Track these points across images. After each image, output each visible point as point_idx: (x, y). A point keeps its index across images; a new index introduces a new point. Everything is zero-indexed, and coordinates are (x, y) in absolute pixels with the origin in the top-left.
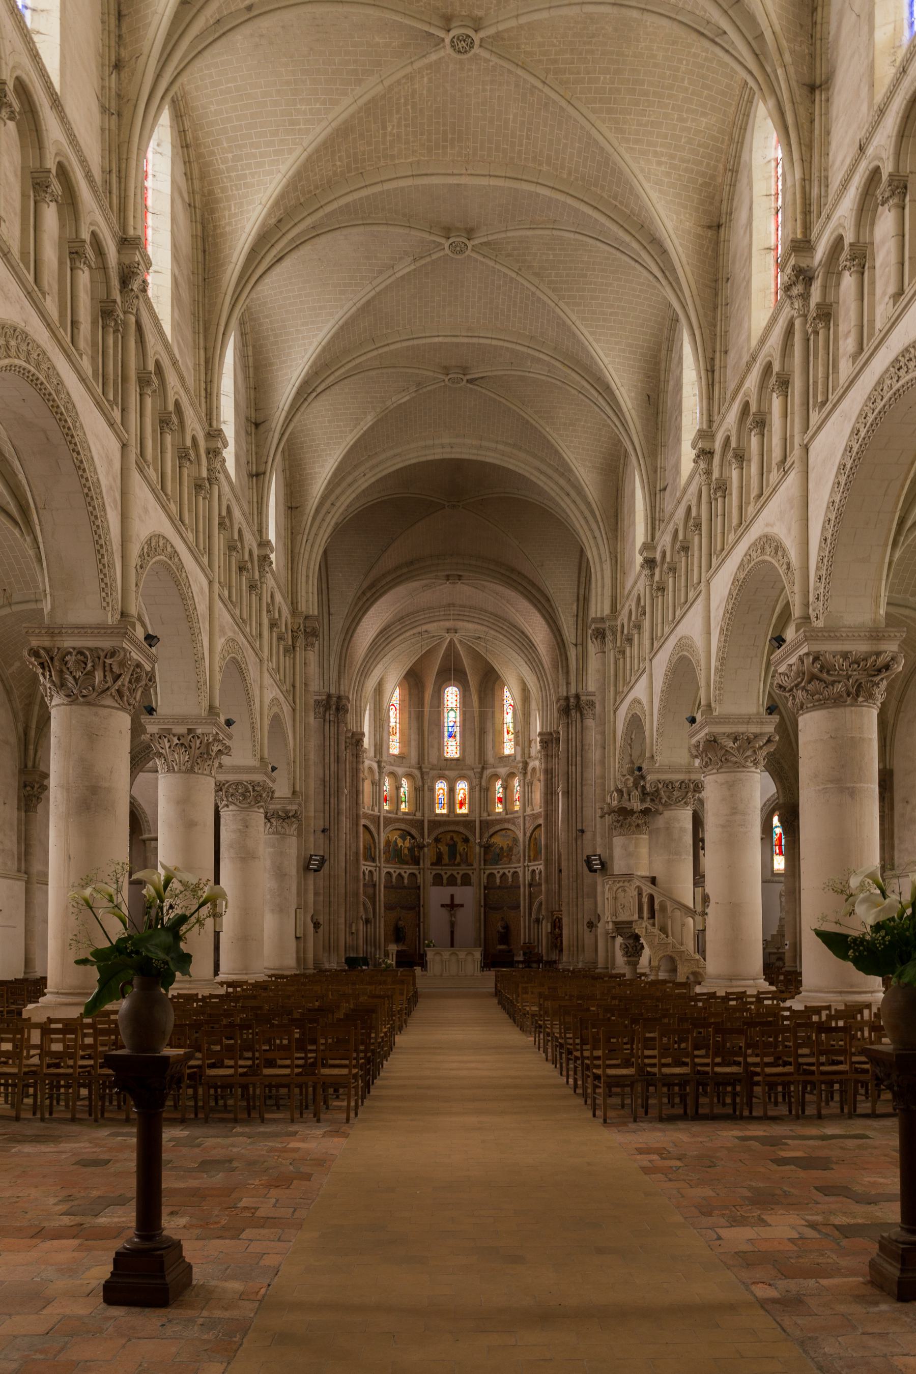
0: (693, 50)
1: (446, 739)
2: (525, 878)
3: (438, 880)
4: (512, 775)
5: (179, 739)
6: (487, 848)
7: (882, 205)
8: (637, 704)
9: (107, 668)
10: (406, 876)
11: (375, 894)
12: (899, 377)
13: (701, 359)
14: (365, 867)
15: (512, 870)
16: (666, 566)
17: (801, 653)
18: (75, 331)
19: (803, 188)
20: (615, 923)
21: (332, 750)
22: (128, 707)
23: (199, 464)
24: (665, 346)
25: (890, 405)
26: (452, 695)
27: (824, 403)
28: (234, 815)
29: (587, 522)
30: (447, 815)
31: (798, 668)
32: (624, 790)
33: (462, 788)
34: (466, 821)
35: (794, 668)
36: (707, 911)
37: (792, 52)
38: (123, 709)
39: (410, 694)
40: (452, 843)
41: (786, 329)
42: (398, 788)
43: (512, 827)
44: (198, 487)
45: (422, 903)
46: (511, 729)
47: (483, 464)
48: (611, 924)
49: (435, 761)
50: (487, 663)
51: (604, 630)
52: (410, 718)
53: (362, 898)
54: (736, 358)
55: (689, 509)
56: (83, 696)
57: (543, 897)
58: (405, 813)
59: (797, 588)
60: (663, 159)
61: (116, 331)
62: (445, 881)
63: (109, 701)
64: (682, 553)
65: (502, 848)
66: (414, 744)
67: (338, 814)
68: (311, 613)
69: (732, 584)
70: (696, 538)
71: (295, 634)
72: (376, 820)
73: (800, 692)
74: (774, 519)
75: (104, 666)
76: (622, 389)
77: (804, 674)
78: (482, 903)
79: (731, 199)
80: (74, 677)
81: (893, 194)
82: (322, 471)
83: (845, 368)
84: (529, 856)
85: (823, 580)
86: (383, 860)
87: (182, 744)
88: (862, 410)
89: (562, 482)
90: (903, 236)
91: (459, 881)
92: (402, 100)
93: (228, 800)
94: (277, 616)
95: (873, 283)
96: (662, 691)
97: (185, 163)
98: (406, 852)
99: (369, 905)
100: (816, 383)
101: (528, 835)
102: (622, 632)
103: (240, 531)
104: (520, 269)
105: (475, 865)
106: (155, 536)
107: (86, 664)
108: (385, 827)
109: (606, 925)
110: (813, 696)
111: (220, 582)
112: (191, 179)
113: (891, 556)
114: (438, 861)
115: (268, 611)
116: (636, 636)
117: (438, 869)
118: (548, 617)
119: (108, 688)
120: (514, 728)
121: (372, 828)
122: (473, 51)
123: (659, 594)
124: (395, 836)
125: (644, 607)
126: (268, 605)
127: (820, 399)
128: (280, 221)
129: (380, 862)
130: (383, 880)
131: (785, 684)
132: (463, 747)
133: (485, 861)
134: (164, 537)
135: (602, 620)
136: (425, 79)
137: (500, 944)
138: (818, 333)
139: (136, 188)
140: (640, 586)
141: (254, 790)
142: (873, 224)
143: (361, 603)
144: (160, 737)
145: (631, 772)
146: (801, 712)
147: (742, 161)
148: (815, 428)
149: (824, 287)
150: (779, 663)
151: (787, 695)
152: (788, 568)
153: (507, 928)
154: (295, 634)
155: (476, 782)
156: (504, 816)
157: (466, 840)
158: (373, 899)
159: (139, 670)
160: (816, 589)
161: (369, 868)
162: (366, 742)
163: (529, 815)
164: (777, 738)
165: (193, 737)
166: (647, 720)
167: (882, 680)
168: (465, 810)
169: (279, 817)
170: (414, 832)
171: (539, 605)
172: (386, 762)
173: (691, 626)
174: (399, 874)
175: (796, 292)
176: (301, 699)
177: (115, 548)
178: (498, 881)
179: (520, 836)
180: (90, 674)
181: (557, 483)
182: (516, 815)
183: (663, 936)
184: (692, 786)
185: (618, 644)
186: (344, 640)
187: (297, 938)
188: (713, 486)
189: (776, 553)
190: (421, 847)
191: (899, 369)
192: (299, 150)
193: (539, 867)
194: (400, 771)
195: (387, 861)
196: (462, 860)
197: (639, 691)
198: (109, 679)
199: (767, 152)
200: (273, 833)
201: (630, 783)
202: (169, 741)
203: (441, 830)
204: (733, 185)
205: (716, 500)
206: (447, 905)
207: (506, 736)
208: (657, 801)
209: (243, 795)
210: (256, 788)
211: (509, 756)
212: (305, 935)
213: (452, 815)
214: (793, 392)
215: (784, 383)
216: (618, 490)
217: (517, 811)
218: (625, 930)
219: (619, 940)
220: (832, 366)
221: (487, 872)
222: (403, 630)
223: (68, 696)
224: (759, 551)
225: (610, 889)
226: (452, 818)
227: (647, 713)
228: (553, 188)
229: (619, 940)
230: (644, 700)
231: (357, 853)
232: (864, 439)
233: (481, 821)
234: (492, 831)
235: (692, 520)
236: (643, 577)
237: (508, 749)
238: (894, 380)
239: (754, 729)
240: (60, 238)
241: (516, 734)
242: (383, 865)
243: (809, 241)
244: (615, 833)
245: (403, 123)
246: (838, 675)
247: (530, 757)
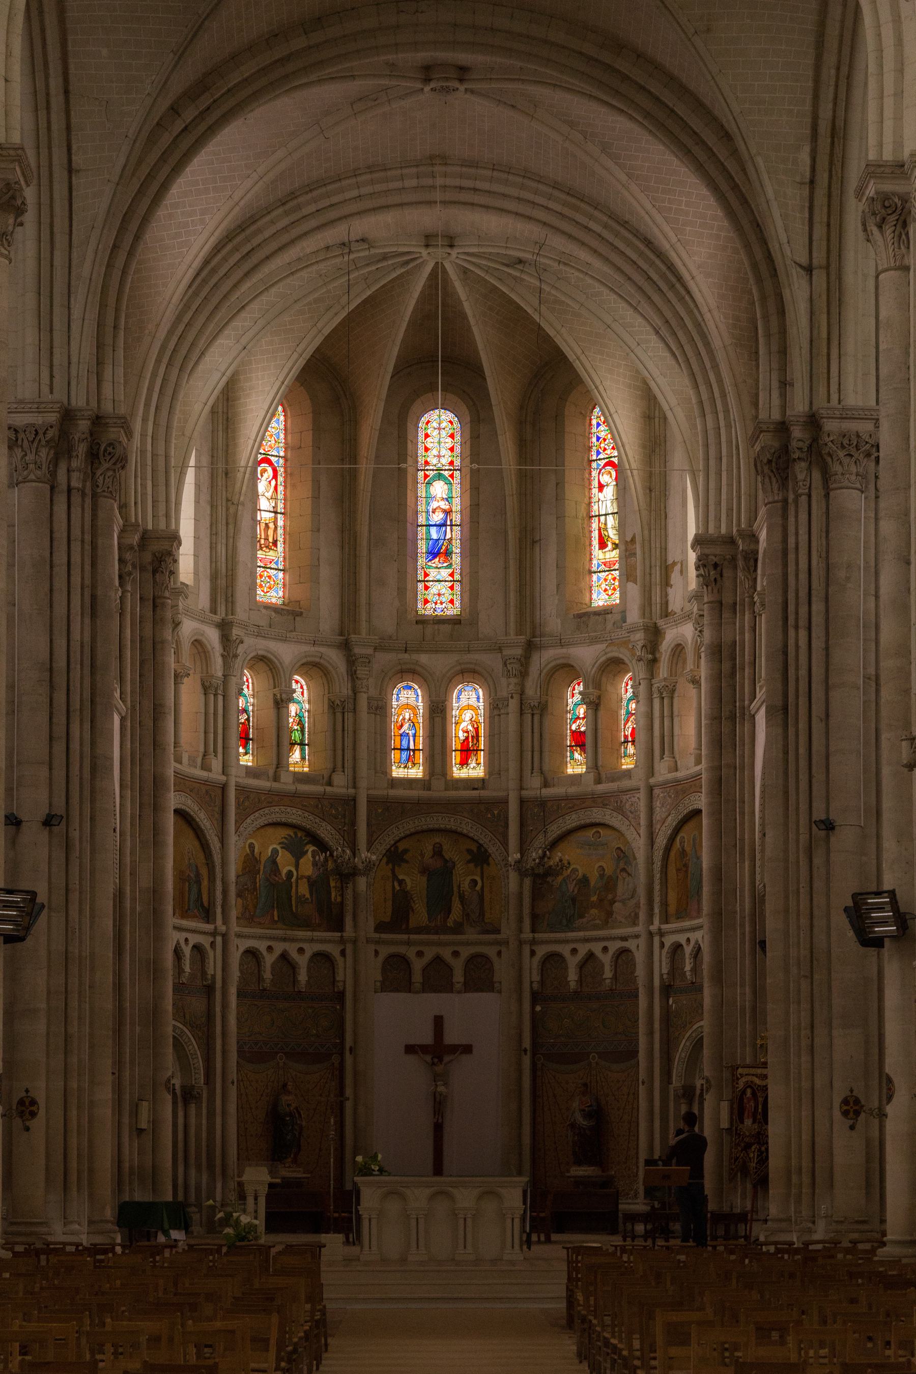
1: (421, 561)
3: (396, 976)
10: (302, 961)
15: (614, 946)
26: (439, 435)
33: (468, 706)
34: (480, 802)
43: (615, 820)
45: (349, 1042)
46: (613, 534)
52: (316, 498)
62: (417, 977)
65: (585, 881)
66: (328, 573)
78: (527, 1043)
84: (665, 904)
86: (234, 914)
91: (458, 977)
98: (304, 889)
99: (193, 1047)
101: (661, 841)
105: (507, 931)
114: (398, 919)
121: (203, 819)
124: (271, 845)
129: (225, 921)
132: (471, 583)
133: (534, 917)
137: (579, 1163)
153: (597, 1114)
155: (508, 686)
156: (590, 786)
157: (480, 857)
161: (194, 939)
163: (664, 785)
168: (475, 770)
170: (326, 831)
174: (284, 956)
176: (225, 1006)
178: (572, 976)
179: (639, 845)
194: (286, 653)
195: (248, 918)
206: (424, 1049)
207: (599, 556)
221: (542, 951)
226: (439, 792)
233: (522, 802)
237: (603, 593)
241: (627, 547)
242: (235, 928)
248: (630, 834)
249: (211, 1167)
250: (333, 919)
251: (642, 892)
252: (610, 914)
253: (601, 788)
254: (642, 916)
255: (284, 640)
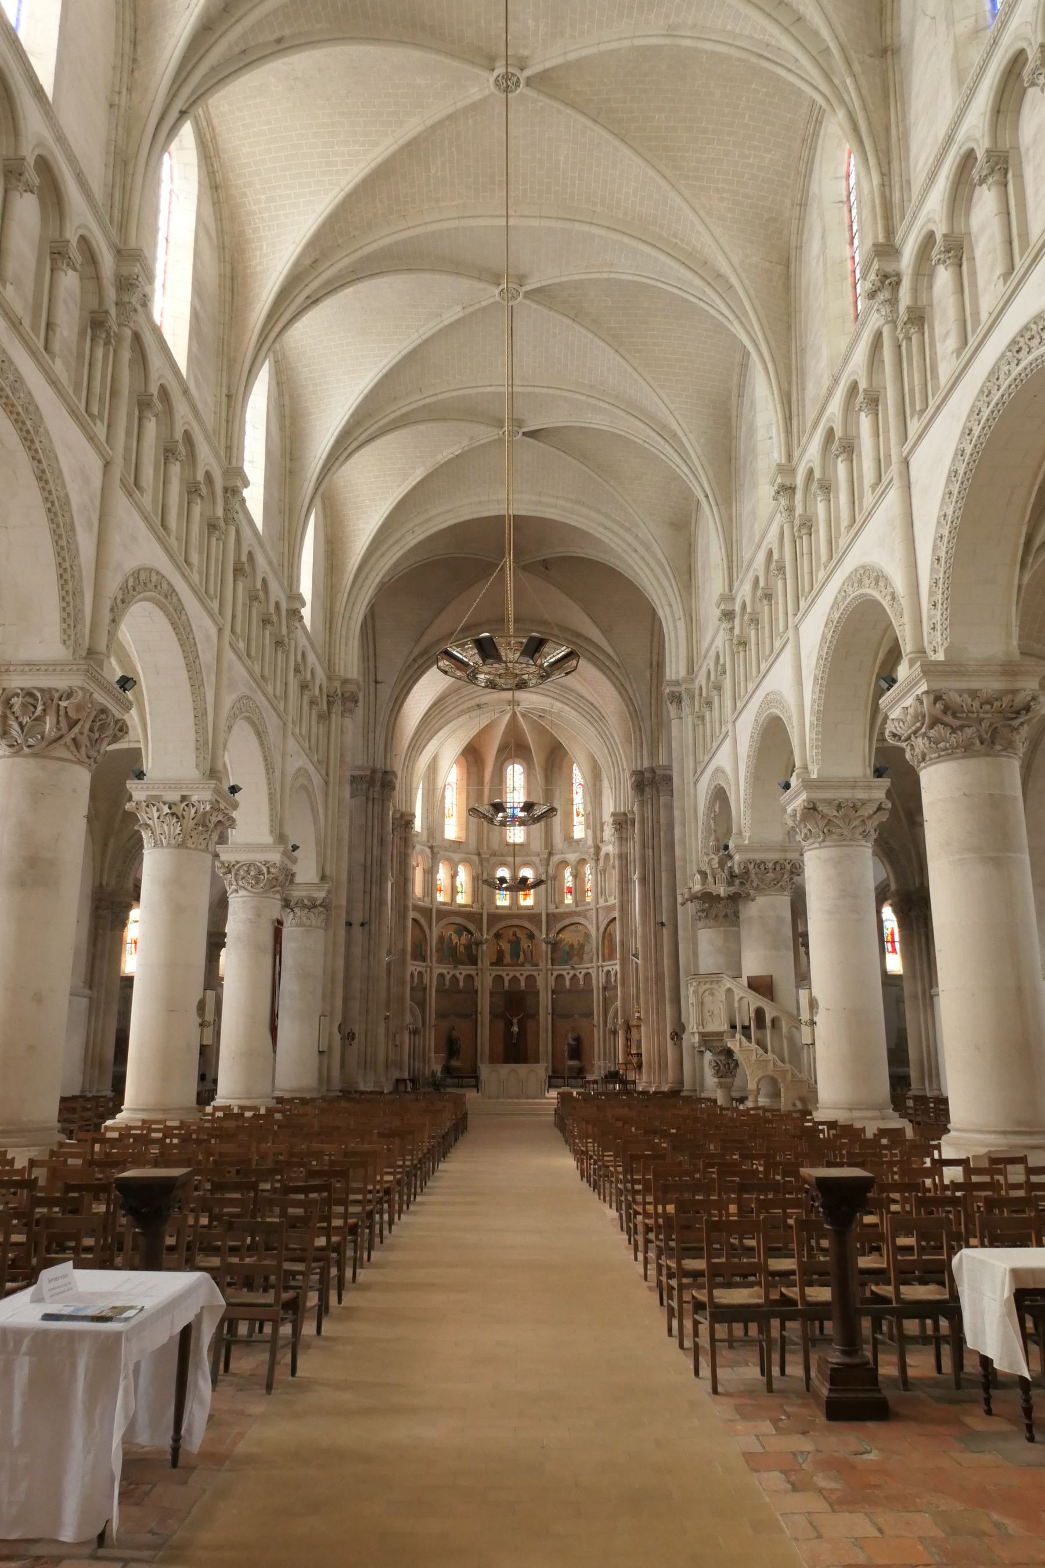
0: (753, 86)
2: (598, 980)
4: (582, 861)
5: (170, 808)
6: (555, 945)
7: (980, 185)
8: (720, 774)
9: (62, 713)
10: (461, 978)
11: (424, 999)
12: (1019, 361)
13: (776, 392)
14: (414, 968)
15: (584, 971)
16: (746, 617)
17: (919, 692)
18: (50, 332)
19: (883, 195)
20: (703, 1035)
21: (376, 832)
22: (87, 760)
23: (214, 502)
24: (735, 392)
25: (1010, 394)
27: (923, 411)
28: (244, 902)
29: (658, 579)
30: (510, 908)
31: (916, 710)
32: (708, 871)
35: (911, 711)
36: (815, 1019)
37: (862, 63)
38: (80, 763)
39: (468, 772)
40: (514, 939)
41: (872, 344)
42: (453, 877)
44: (212, 527)
46: (582, 811)
47: (543, 521)
48: (697, 1036)
49: (495, 845)
50: (552, 735)
51: (680, 694)
53: (408, 1003)
54: (814, 388)
55: (770, 553)
56: (29, 746)
57: (619, 1003)
58: (461, 906)
59: (906, 618)
60: (725, 195)
61: (107, 343)
63: (65, 754)
64: (765, 602)
67: (380, 904)
68: (350, 676)
69: (826, 626)
70: (780, 583)
71: (331, 699)
72: (427, 912)
73: (920, 739)
74: (875, 547)
75: (58, 710)
76: (691, 436)
77: (924, 717)
78: (550, 1011)
79: (800, 232)
80: (20, 724)
81: (992, 171)
82: (364, 527)
83: (946, 370)
84: (603, 955)
85: (939, 606)
87: (173, 814)
88: (973, 406)
89: (630, 538)
90: (1008, 214)
92: (446, 143)
93: (237, 884)
94: (309, 676)
95: (973, 274)
96: (749, 756)
97: (214, 204)
98: (462, 949)
99: (418, 1012)
100: (912, 391)
101: (602, 930)
102: (701, 695)
103: (303, 654)
104: (576, 316)
105: (542, 965)
106: (146, 569)
107: (35, 707)
108: (438, 920)
109: (691, 1038)
110: (937, 743)
111: (233, 631)
112: (221, 220)
113: (1020, 579)
114: (499, 961)
115: (297, 670)
116: (716, 698)
117: (498, 971)
118: (618, 685)
119: (61, 737)
120: (585, 809)
121: (423, 921)
122: (519, 90)
123: (741, 648)
124: (450, 932)
125: (724, 666)
126: (296, 664)
127: (919, 403)
128: (316, 261)
130: (435, 982)
131: (899, 732)
133: (552, 959)
134: (158, 573)
135: (677, 683)
136: (470, 121)
138: (910, 339)
139: (396, 542)
140: (719, 642)
141: (269, 872)
142: (968, 214)
143: (411, 671)
144: (147, 806)
145: (717, 850)
146: (923, 765)
147: (811, 193)
148: (916, 436)
149: (915, 291)
150: (892, 707)
151: (904, 745)
152: (893, 599)
153: (578, 1039)
154: (331, 699)
156: (573, 908)
157: (531, 936)
158: (422, 1005)
159: (104, 716)
160: (930, 618)
161: (419, 969)
162: (418, 825)
163: (602, 908)
164: (889, 806)
165: (187, 805)
166: (733, 792)
167: (1022, 724)
169: (305, 906)
170: (471, 926)
171: (608, 672)
172: (440, 847)
173: (780, 680)
174: (454, 976)
175: (882, 298)
176: (430, 996)
177: (84, 574)
178: (568, 983)
179: (593, 932)
180: (40, 719)
181: (624, 540)
182: (588, 907)
183: (761, 1051)
184: (788, 867)
185: (697, 709)
186: (392, 710)
187: (320, 1052)
188: (797, 522)
189: (877, 584)
190: (478, 944)
191: (1018, 352)
192: (337, 189)
193: (615, 967)
195: (440, 961)
196: (526, 959)
197: (723, 759)
198: (64, 724)
199: (841, 171)
200: (297, 925)
201: (715, 864)
202: (158, 810)
203: (502, 924)
204: (801, 219)
205: (801, 538)
208: (748, 885)
209: (255, 877)
210: (272, 870)
211: (580, 840)
212: (330, 1048)
213: (515, 908)
214: (886, 410)
215: (874, 401)
216: (690, 545)
217: (589, 903)
218: (715, 1044)
219: (708, 1056)
220: (929, 371)
221: (555, 974)
222: (460, 702)
223: (11, 746)
224: (856, 585)
225: (695, 992)
226: (515, 911)
227: (732, 782)
228: (608, 228)
229: (708, 1056)
230: (729, 769)
231: (404, 950)
232: (979, 437)
233: (547, 915)
234: (559, 926)
235: (774, 564)
236: (721, 632)
237: (579, 832)
238: (1013, 364)
239: (861, 795)
240: (41, 237)
241: (587, 816)
243: (892, 246)
244: (700, 924)
245: (448, 165)
246: (967, 718)
247: (602, 841)
248: (589, 927)
249: (424, 1061)
250: (473, 961)
251: (594, 950)
252: (582, 959)
253: (578, 909)
254: (595, 958)
255: (455, 852)
